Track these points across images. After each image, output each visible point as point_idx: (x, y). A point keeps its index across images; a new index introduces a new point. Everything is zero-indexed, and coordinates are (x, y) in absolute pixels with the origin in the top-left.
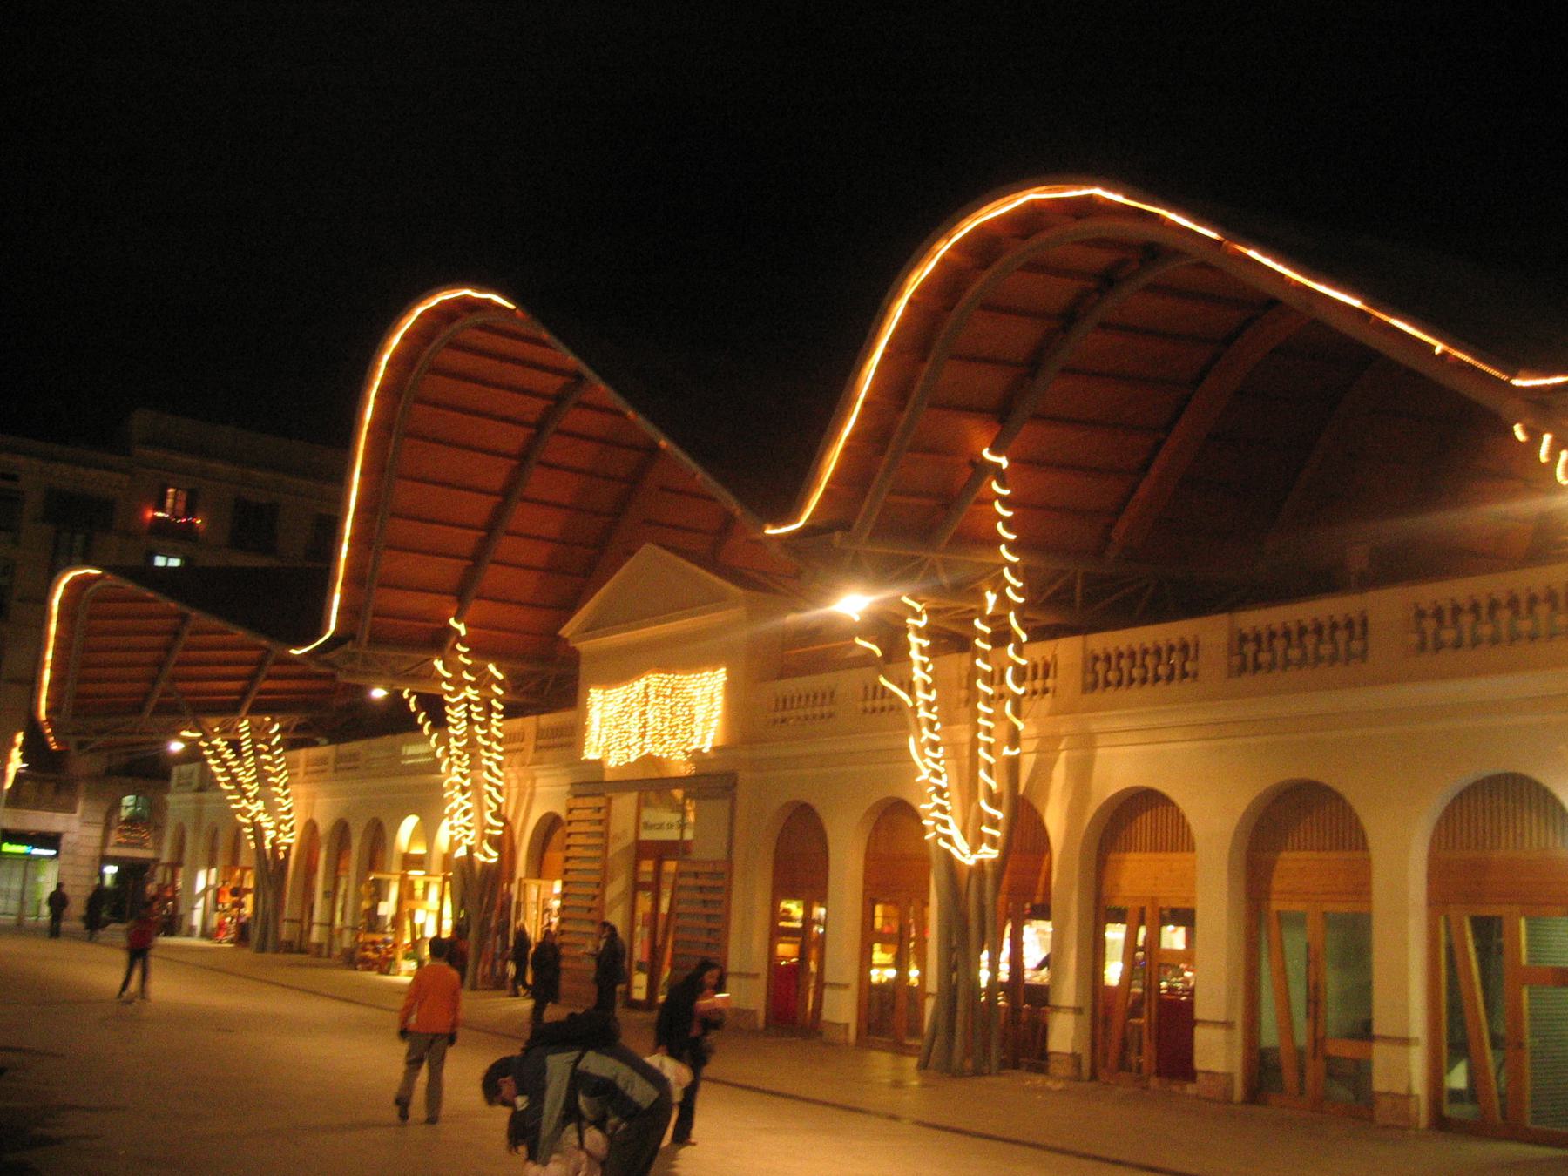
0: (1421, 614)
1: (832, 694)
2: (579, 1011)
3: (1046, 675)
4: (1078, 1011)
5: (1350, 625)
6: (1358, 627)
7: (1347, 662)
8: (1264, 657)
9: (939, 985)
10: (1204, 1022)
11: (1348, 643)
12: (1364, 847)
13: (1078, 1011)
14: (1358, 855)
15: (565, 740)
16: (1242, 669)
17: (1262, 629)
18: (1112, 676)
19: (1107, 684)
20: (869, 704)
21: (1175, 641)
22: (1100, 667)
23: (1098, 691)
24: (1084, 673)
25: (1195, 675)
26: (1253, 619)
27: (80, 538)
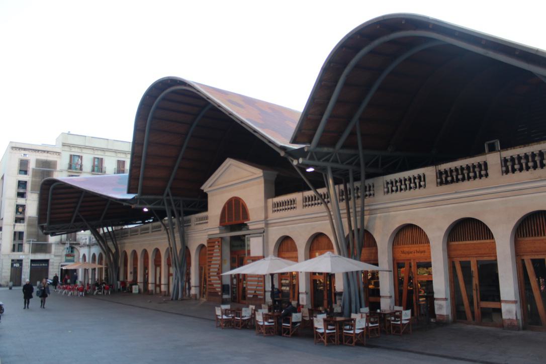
0: (388, 183)
1: (294, 201)
2: (83, 231)
3: (370, 190)
4: (307, 293)
5: (419, 177)
6: (293, 202)
7: (480, 178)
8: (449, 179)
9: (312, 306)
10: (383, 297)
11: (410, 185)
12: (493, 238)
13: (307, 293)
14: (492, 241)
15: (205, 221)
16: (507, 172)
17: (448, 169)
18: (394, 188)
19: (392, 191)
20: (276, 209)
21: (416, 176)
22: (390, 186)
23: (390, 194)
24: (502, 167)
25: (374, 195)
26: (444, 167)
27: (344, 331)
